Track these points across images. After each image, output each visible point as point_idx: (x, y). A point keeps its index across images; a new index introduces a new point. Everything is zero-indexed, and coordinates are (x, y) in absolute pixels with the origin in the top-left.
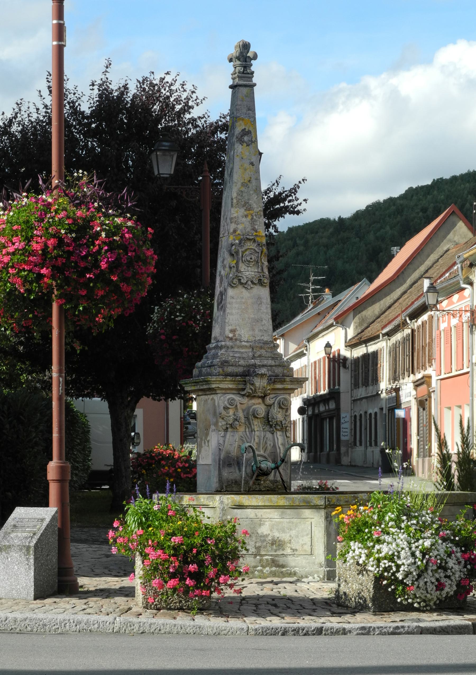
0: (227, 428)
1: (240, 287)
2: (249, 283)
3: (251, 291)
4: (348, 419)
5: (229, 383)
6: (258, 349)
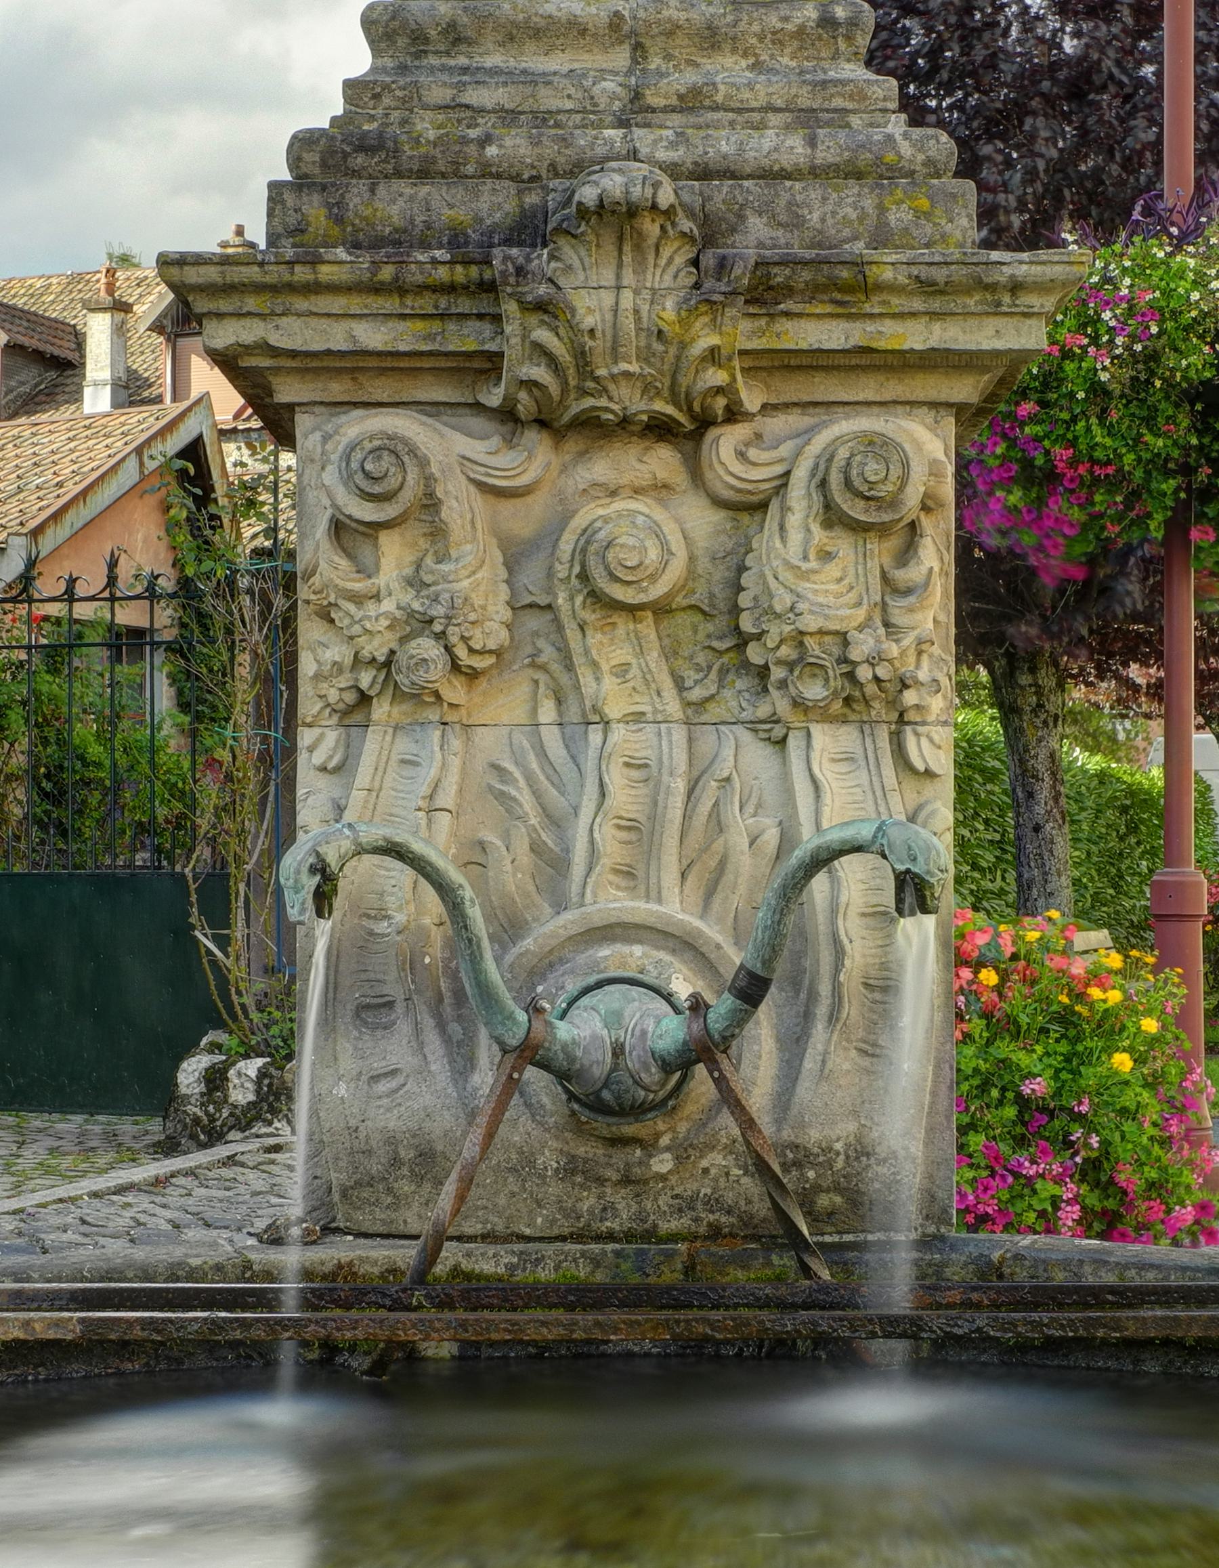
0: (364, 699)
5: (355, 303)
6: (682, 47)
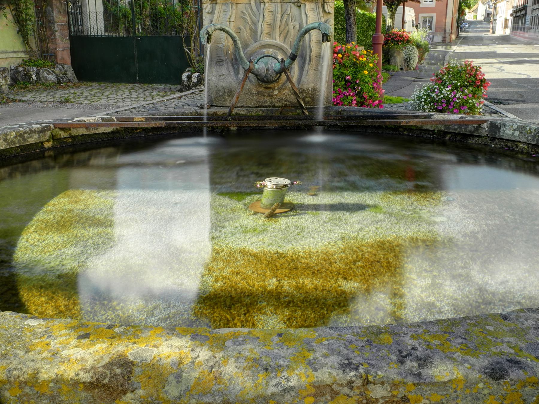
4: (529, 18)
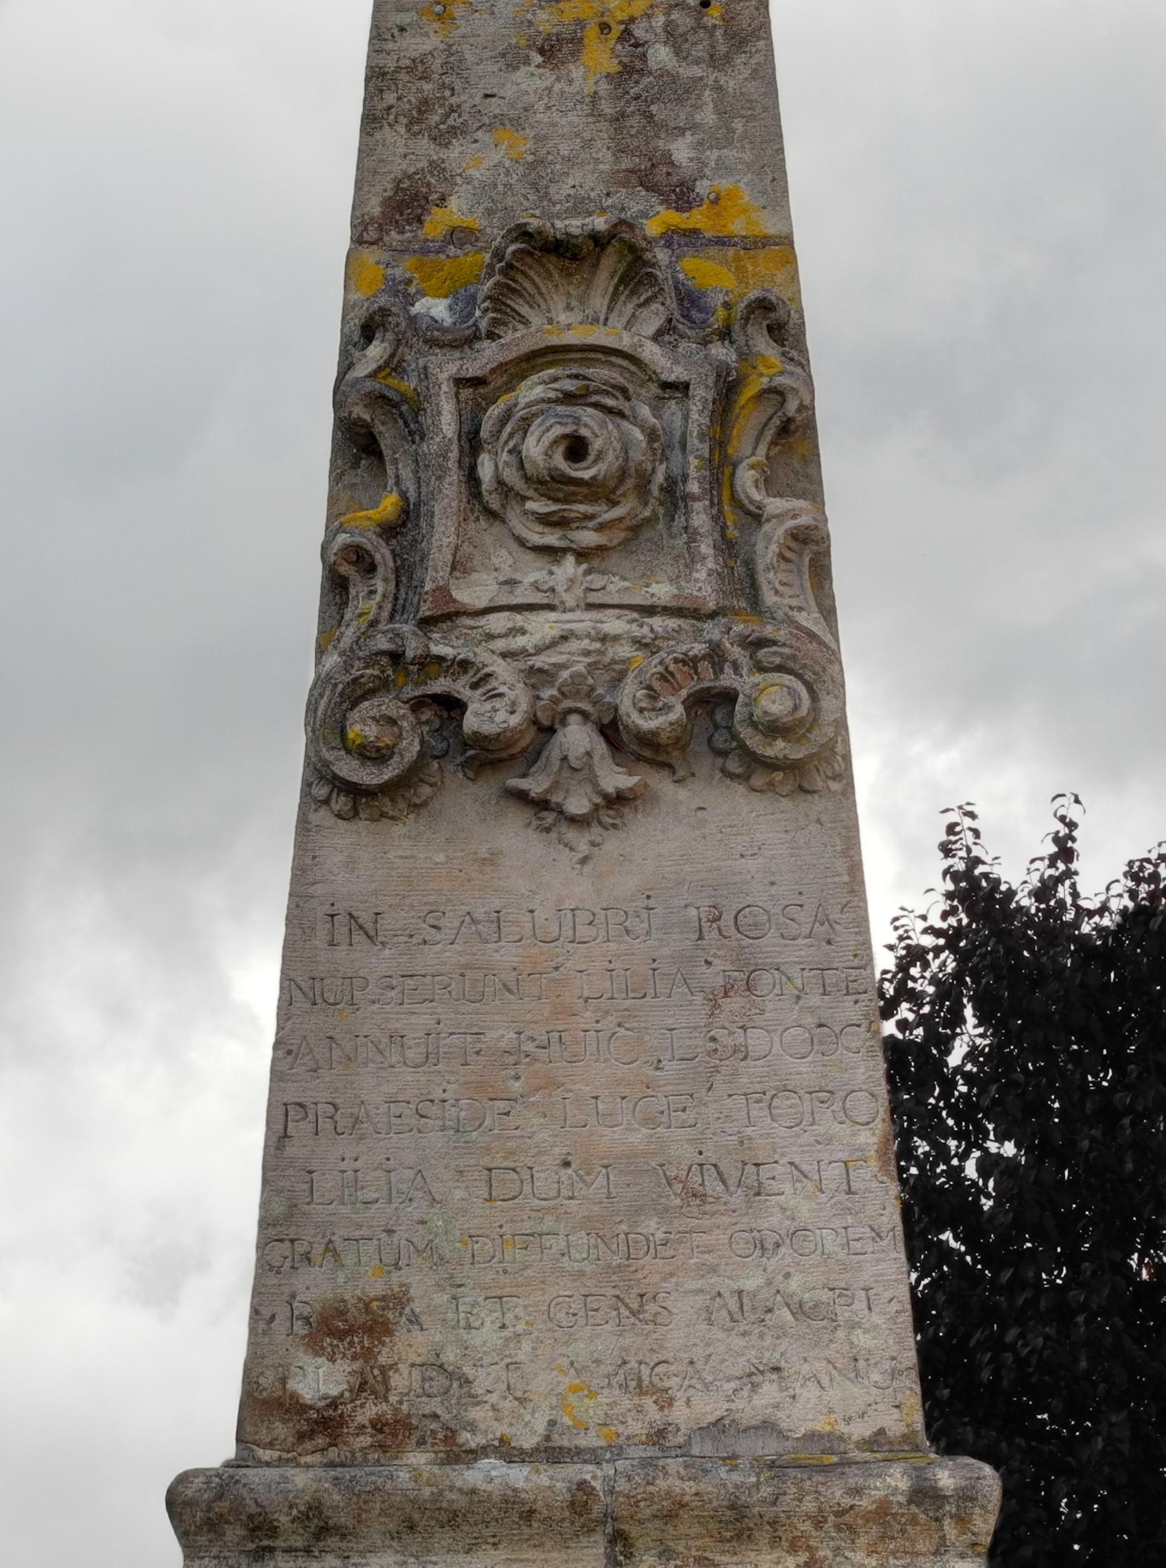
1: (464, 801)
2: (577, 737)
3: (613, 844)
